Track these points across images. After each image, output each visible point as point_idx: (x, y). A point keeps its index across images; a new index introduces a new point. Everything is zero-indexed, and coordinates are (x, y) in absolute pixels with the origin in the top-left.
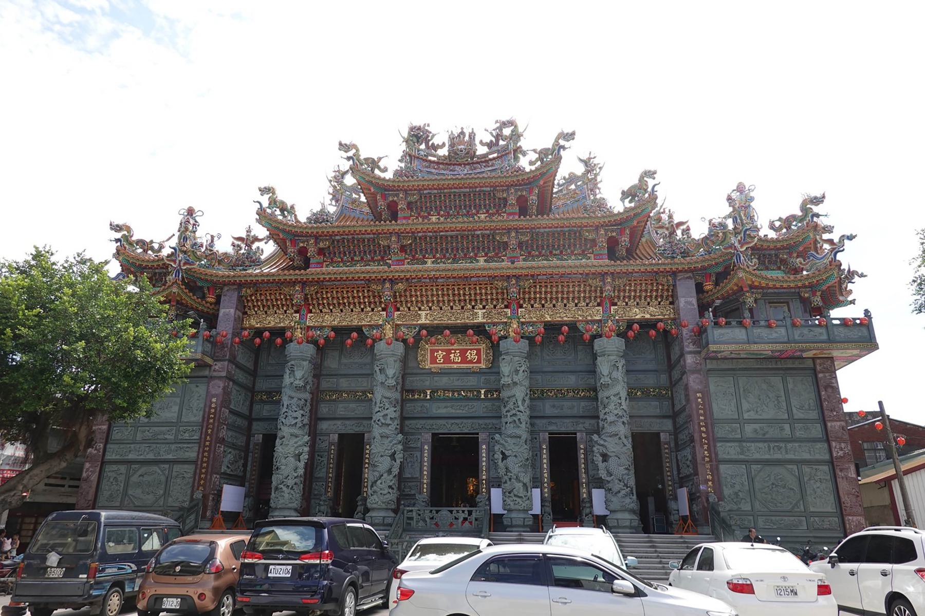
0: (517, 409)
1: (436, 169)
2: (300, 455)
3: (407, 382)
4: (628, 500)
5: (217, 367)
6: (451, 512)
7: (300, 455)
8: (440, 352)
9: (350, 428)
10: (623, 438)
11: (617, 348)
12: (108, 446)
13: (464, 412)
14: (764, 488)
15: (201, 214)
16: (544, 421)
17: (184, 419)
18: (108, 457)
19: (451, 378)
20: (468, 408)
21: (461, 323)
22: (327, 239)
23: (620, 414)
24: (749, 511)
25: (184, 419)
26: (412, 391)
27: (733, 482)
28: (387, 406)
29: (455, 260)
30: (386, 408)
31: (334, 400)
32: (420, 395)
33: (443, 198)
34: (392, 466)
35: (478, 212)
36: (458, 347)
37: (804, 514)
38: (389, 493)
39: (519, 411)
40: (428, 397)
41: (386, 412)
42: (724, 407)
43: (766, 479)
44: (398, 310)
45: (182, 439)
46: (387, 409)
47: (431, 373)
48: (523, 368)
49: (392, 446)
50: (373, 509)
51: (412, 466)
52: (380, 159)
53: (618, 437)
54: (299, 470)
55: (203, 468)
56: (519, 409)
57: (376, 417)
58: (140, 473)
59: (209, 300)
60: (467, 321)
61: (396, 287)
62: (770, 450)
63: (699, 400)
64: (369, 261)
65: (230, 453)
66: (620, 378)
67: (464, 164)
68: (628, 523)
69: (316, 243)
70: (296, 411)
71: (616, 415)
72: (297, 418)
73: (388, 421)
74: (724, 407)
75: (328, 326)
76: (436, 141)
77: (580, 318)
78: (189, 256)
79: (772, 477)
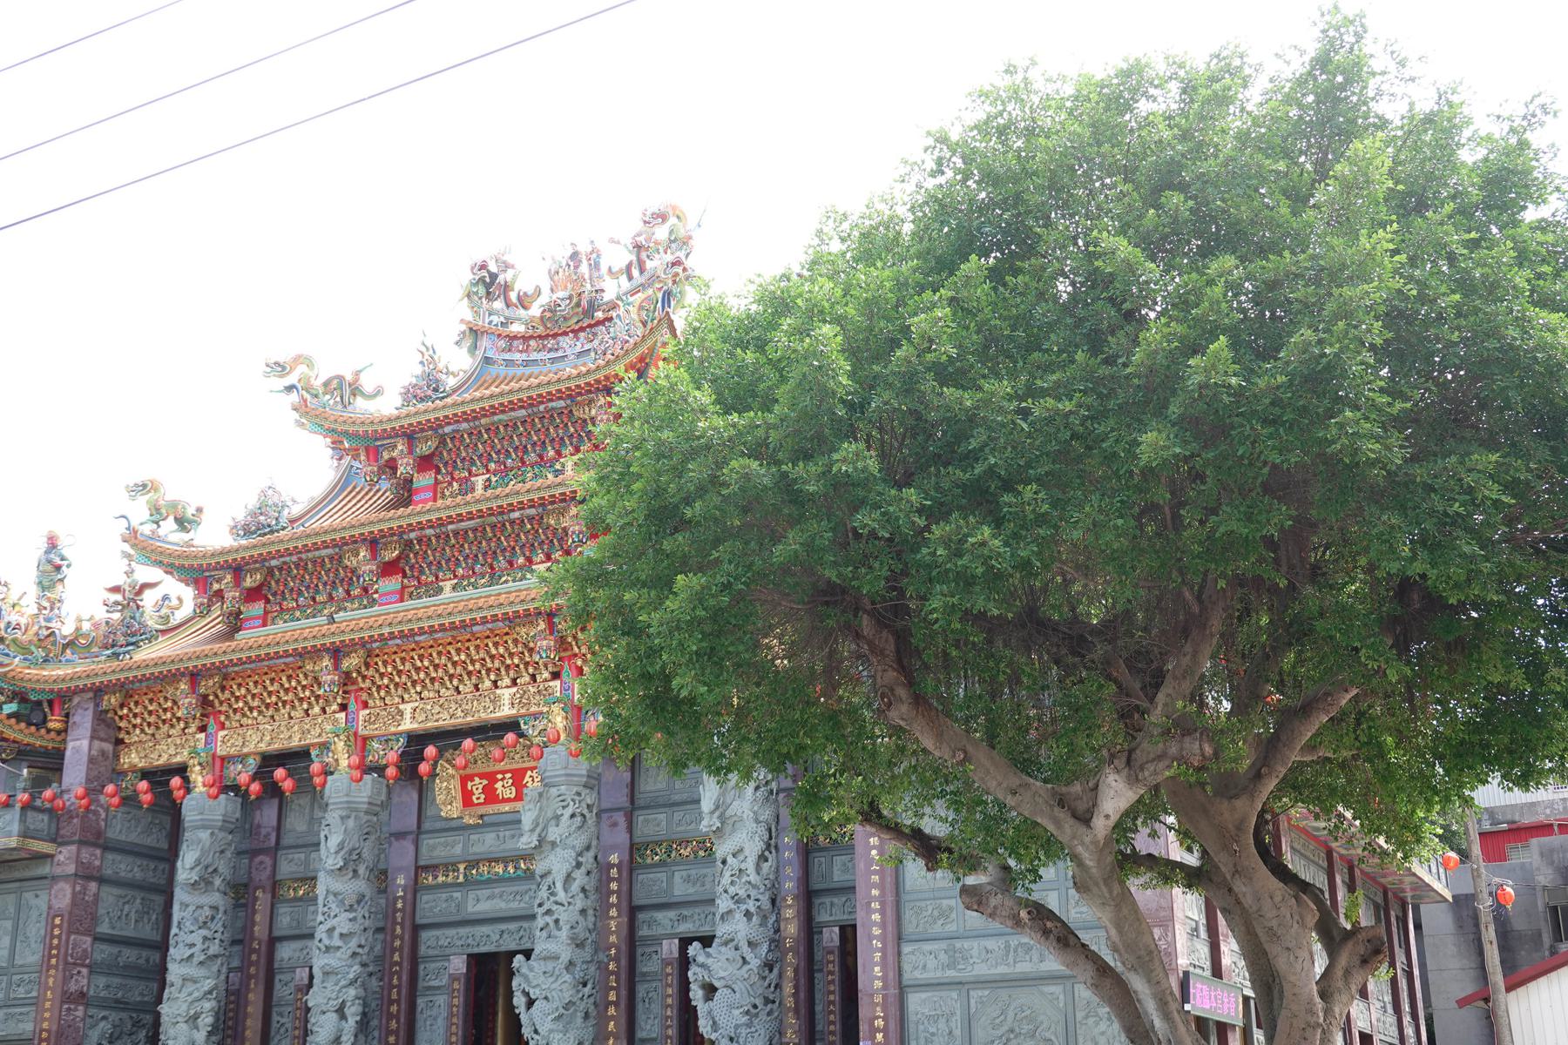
0: (552, 899)
1: (521, 352)
2: (196, 1017)
3: (424, 850)
5: (61, 858)
7: (196, 1017)
8: (477, 780)
9: (489, 940)
10: (745, 949)
13: (522, 905)
16: (672, 914)
17: (18, 961)
19: (501, 834)
22: (257, 569)
23: (742, 893)
25: (18, 961)
26: (432, 868)
28: (335, 909)
29: (494, 579)
30: (332, 914)
31: (301, 899)
33: (486, 436)
35: (559, 454)
36: (509, 767)
39: (556, 903)
40: (461, 879)
41: (335, 922)
43: (997, 1021)
44: (365, 705)
45: (15, 999)
47: (458, 828)
48: (569, 811)
49: (339, 991)
53: (731, 945)
56: (557, 898)
57: (320, 933)
59: (51, 725)
60: (483, 715)
61: (346, 664)
64: (344, 600)
65: (104, 1018)
67: (572, 331)
69: (238, 580)
71: (733, 898)
72: (194, 945)
73: (337, 942)
75: (255, 754)
76: (523, 285)
78: (8, 646)
79: (1011, 1015)
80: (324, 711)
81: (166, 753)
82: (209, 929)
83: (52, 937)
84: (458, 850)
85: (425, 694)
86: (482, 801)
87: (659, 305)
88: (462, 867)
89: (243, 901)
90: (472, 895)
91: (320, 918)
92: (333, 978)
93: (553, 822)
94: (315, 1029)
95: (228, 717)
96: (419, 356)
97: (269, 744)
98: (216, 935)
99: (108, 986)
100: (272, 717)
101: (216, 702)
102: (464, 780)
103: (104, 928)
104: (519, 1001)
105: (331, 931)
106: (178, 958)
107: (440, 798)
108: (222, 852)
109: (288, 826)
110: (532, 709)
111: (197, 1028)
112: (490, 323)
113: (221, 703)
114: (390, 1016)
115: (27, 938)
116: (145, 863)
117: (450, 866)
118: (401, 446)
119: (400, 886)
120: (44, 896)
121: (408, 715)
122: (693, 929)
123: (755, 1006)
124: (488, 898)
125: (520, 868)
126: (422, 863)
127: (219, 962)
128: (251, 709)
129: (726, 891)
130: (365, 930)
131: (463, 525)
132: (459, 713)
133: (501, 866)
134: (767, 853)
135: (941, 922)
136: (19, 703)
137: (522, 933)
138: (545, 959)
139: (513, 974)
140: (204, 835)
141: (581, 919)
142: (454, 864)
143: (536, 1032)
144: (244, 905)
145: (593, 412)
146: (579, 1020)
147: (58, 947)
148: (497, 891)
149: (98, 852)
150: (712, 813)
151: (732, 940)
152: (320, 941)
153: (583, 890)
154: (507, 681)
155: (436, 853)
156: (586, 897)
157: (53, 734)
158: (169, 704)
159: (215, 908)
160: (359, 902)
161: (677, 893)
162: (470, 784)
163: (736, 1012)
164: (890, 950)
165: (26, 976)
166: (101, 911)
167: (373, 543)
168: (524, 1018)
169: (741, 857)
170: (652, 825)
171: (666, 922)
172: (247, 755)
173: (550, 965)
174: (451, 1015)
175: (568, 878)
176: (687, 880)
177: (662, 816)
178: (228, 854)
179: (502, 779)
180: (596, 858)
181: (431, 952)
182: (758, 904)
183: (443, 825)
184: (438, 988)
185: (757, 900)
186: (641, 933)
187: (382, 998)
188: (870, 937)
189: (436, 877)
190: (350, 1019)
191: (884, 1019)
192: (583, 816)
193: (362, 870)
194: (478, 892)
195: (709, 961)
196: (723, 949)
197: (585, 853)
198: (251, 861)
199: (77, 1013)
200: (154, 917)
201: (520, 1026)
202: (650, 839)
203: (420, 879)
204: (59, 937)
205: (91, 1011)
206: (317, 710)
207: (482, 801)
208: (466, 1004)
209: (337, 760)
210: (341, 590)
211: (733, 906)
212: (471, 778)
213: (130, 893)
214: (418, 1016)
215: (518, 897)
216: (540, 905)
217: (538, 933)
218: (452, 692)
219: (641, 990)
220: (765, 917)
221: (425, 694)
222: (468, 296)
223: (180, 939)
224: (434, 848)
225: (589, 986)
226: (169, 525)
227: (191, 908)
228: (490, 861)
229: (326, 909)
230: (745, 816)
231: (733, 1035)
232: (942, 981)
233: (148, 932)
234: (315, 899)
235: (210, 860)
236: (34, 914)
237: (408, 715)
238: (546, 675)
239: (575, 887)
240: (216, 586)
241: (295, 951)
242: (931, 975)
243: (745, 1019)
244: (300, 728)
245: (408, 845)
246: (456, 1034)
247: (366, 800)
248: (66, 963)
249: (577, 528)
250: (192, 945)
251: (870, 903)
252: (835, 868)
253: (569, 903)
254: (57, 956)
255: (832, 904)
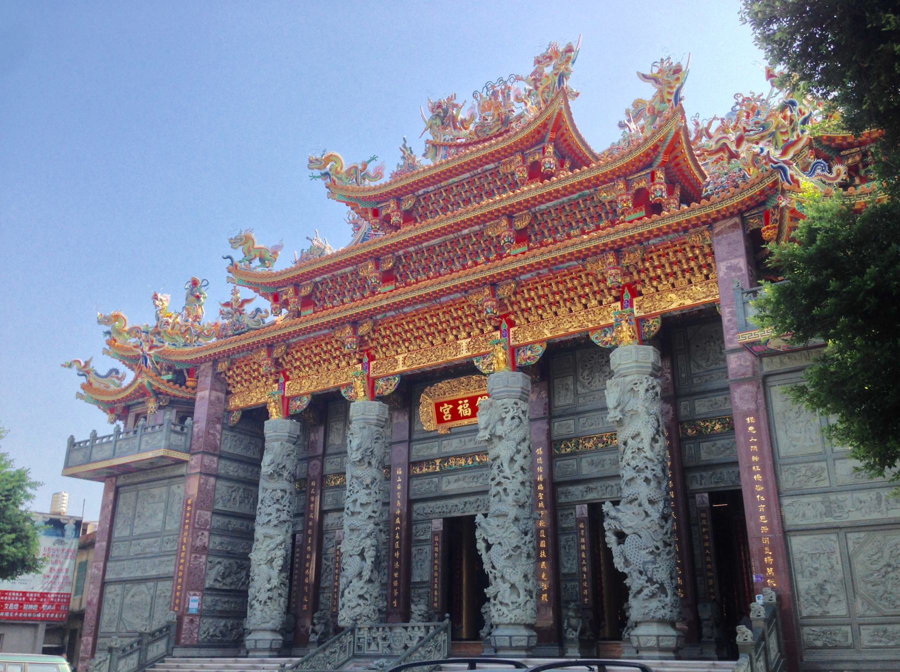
0: (501, 474)
2: (271, 561)
3: (413, 452)
4: (654, 604)
6: (406, 628)
8: (446, 405)
9: (457, 508)
10: (647, 506)
11: (637, 361)
12: (109, 564)
13: (478, 484)
14: (872, 575)
15: (205, 283)
16: (581, 488)
17: (168, 528)
18: (109, 576)
19: (462, 439)
20: (484, 479)
21: (444, 362)
22: (308, 284)
23: (641, 465)
24: (842, 617)
26: (419, 463)
27: (815, 566)
28: (357, 488)
30: (355, 491)
31: (338, 486)
32: (429, 468)
34: (362, 568)
36: (466, 396)
37: (847, 620)
38: (359, 605)
39: (505, 477)
40: (438, 469)
42: (798, 435)
43: (875, 557)
45: (165, 552)
46: (357, 492)
47: (435, 437)
48: (511, 414)
49: (360, 541)
50: (254, 630)
51: (421, 565)
52: (365, 165)
53: (636, 502)
54: (273, 581)
55: (178, 584)
58: (131, 593)
60: (449, 358)
62: (879, 504)
63: (751, 428)
65: (219, 563)
66: (641, 409)
68: (652, 642)
70: (270, 506)
71: (634, 469)
73: (358, 508)
74: (798, 435)
77: (590, 326)
80: (348, 364)
81: (255, 398)
82: (280, 504)
83: (186, 511)
84: (435, 451)
85: (411, 347)
86: (449, 418)
87: (557, 84)
88: (438, 462)
89: (304, 489)
90: (445, 479)
91: (348, 494)
92: (356, 533)
93: (499, 423)
94: (345, 567)
95: (291, 372)
96: (401, 154)
97: (316, 387)
98: (285, 508)
99: (222, 543)
100: (317, 370)
101: (284, 363)
102: (438, 405)
103: (219, 506)
104: (481, 545)
105: (355, 501)
106: (261, 523)
107: (423, 418)
108: (289, 455)
109: (330, 442)
110: (482, 351)
111: (272, 567)
112: (445, 140)
113: (287, 363)
114: (395, 559)
115: (172, 513)
116: (246, 467)
117: (430, 461)
118: (393, 205)
119: (399, 475)
120: (182, 487)
121: (400, 362)
122: (597, 497)
123: (657, 548)
124: (456, 481)
125: (476, 461)
126: (412, 460)
127: (287, 525)
128: (304, 366)
129: (628, 465)
130: (377, 501)
131: (432, 242)
132: (434, 358)
133: (463, 460)
134: (657, 437)
135: (815, 480)
136: (173, 374)
137: (479, 503)
138: (498, 516)
139: (476, 527)
140: (276, 444)
141: (521, 488)
142: (433, 460)
143: (493, 567)
144: (304, 492)
145: (513, 167)
146: (524, 559)
147: (189, 518)
148: (461, 476)
149: (215, 459)
150: (616, 408)
151: (636, 499)
152: (348, 509)
153: (522, 469)
154: (464, 334)
155: (421, 453)
156: (524, 473)
157: (190, 389)
158: (256, 366)
159: (284, 491)
160: (372, 483)
161: (584, 473)
162: (441, 408)
163: (644, 552)
164: (773, 503)
165: (171, 537)
166: (217, 496)
167: (377, 258)
168: (485, 558)
169: (638, 440)
170: (563, 428)
171: (577, 493)
172: (303, 395)
173: (501, 520)
174: (434, 558)
175: (512, 460)
176: (592, 463)
177: (572, 422)
178: (292, 457)
179: (463, 404)
180: (529, 447)
181: (419, 517)
182: (654, 473)
183: (426, 435)
184: (426, 540)
185: (653, 470)
186: (560, 501)
187: (389, 548)
188: (754, 493)
189: (421, 469)
190: (367, 560)
191: (772, 556)
192: (519, 418)
193: (374, 462)
194: (449, 477)
195: (620, 515)
196: (629, 506)
197: (522, 444)
198: (309, 464)
199: (201, 560)
200: (252, 500)
201: (482, 563)
202: (563, 437)
203: (411, 471)
204: (190, 512)
205: (211, 559)
206: (344, 363)
207: (449, 418)
208: (443, 551)
209: (357, 393)
210: (358, 294)
211: (635, 475)
212: (442, 404)
213: (237, 485)
214: (414, 560)
215: (475, 480)
216: (493, 479)
217: (492, 499)
218: (429, 344)
219: (563, 539)
220: (659, 483)
221: (411, 347)
222: (431, 127)
223: (262, 511)
224: (420, 450)
225: (529, 535)
226: (256, 262)
227: (270, 491)
228: (456, 456)
229: (351, 488)
230: (639, 410)
231: (642, 569)
232: (822, 526)
233: (245, 509)
234: (345, 486)
235: (280, 460)
236: (177, 497)
237: (400, 362)
238: (490, 328)
239: (517, 467)
240: (284, 297)
241: (335, 519)
242: (811, 521)
243: (650, 557)
244: (334, 376)
245: (403, 448)
246: (437, 571)
247: (376, 417)
248: (194, 528)
249: (507, 233)
250: (270, 514)
251: (751, 467)
252: (702, 452)
253: (513, 477)
254: (189, 524)
255: (701, 476)
